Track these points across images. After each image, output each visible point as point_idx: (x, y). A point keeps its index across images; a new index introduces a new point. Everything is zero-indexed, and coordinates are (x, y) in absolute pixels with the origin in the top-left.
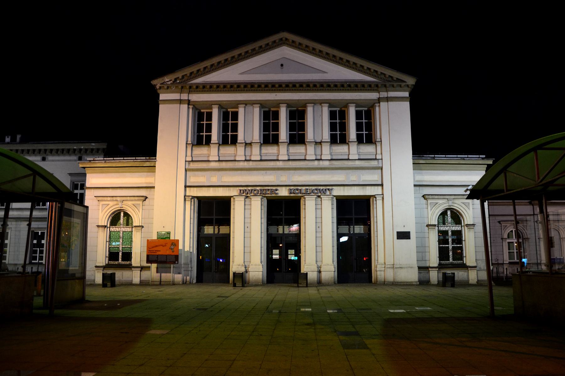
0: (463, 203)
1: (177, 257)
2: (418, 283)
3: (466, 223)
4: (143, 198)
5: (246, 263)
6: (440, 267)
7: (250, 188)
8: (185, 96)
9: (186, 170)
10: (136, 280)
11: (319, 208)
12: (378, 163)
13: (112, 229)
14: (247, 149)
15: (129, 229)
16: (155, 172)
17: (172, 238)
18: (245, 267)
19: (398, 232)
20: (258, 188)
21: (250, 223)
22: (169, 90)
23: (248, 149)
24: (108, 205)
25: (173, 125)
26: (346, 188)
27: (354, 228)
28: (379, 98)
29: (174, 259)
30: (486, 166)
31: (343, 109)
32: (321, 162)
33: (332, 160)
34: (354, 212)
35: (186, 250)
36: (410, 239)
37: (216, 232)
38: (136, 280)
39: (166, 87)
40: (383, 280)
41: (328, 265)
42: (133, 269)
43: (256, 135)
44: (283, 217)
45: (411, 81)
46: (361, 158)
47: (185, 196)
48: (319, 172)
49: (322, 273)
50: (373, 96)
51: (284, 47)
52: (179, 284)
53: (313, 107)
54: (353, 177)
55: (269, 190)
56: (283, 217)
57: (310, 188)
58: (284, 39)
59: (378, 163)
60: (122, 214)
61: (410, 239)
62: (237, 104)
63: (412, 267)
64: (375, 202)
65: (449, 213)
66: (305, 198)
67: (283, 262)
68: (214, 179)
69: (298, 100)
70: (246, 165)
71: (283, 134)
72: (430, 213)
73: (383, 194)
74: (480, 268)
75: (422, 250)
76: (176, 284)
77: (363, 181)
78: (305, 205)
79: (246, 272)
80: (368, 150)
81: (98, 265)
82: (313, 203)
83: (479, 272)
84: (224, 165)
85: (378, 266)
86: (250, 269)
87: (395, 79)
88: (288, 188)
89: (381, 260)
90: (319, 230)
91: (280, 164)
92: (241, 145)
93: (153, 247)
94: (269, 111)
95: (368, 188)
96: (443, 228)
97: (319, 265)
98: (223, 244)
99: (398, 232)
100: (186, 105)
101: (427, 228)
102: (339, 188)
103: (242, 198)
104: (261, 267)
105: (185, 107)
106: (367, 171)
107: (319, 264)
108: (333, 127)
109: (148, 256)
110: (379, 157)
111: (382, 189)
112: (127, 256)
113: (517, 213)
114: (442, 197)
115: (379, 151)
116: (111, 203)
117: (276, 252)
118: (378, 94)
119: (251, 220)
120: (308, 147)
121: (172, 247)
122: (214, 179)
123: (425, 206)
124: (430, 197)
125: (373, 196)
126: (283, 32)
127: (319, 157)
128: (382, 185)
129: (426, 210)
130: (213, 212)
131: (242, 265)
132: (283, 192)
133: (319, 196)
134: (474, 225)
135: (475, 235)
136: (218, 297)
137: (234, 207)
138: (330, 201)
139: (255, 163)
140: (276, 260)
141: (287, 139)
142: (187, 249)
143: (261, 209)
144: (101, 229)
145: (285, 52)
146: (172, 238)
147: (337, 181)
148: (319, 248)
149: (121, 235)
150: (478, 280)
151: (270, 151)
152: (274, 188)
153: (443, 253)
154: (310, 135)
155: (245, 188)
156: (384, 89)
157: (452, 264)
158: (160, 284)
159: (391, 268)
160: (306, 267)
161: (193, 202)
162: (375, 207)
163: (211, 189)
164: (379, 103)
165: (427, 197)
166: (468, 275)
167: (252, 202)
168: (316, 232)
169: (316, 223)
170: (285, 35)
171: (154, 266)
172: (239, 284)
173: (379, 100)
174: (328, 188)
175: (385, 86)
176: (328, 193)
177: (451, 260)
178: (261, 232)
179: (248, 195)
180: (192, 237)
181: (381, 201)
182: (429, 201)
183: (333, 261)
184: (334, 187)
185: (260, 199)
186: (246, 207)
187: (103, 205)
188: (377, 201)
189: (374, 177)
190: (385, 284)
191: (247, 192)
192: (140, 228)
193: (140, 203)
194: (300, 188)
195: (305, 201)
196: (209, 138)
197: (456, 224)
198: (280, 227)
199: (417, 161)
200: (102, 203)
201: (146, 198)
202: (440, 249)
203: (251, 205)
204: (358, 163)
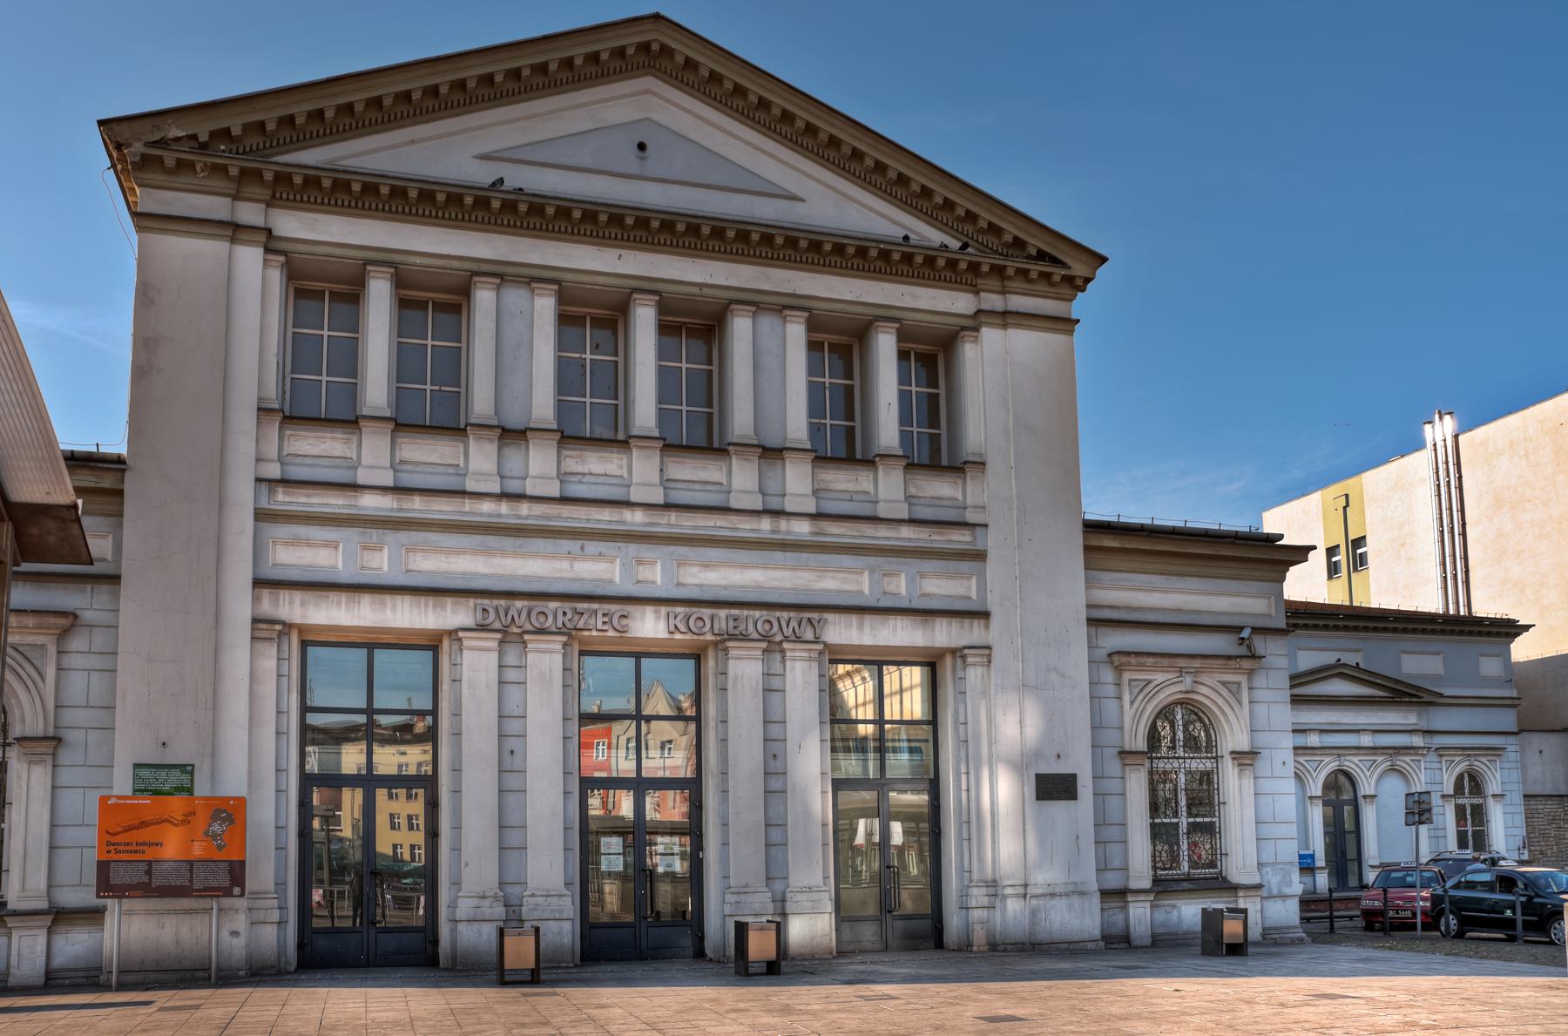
0: (1224, 683)
8: (250, 213)
26: (868, 618)
28: (979, 312)
29: (224, 881)
32: (783, 524)
33: (818, 516)
50: (957, 303)
84: (417, 506)
87: (1033, 252)
103: (491, 640)
104: (567, 901)
109: (103, 867)
113: (381, 656)
121: (216, 828)
124: (1133, 660)
131: (496, 897)
139: (539, 509)
156: (994, 283)
157: (1188, 878)
163: (366, 599)
173: (979, 318)
175: (998, 271)
177: (1185, 866)
184: (830, 617)
191: (510, 613)
199: (1094, 542)
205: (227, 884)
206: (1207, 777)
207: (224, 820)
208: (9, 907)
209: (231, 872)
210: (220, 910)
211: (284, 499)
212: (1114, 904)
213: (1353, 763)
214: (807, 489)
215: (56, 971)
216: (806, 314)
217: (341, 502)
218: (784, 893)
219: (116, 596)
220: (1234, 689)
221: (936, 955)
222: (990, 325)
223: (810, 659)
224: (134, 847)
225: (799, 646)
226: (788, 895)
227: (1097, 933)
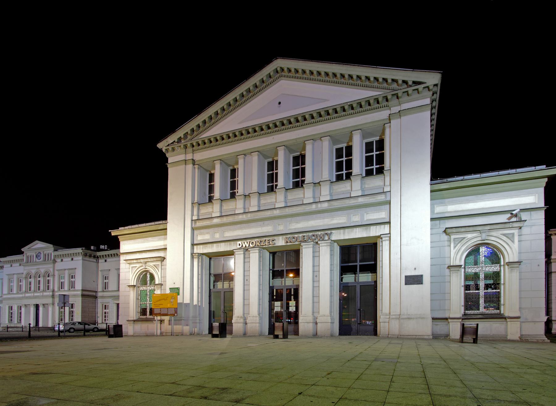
0: (504, 235)
2: (431, 337)
3: (507, 261)
11: (316, 256)
12: (386, 197)
19: (406, 277)
22: (175, 152)
26: (347, 230)
30: (546, 180)
32: (319, 205)
34: (359, 258)
36: (422, 283)
39: (170, 149)
41: (325, 316)
45: (433, 78)
48: (322, 218)
50: (383, 114)
51: (282, 81)
52: (186, 335)
53: (313, 145)
59: (386, 197)
61: (422, 283)
62: (237, 155)
70: (244, 217)
71: (381, 198)
72: (453, 251)
75: (439, 295)
76: (321, 337)
77: (367, 220)
80: (375, 182)
82: (311, 250)
83: (523, 324)
84: (225, 220)
90: (316, 279)
91: (277, 213)
92: (240, 197)
95: (372, 228)
99: (406, 277)
101: (447, 270)
102: (338, 231)
105: (190, 166)
114: (471, 229)
115: (387, 183)
116: (138, 265)
117: (277, 304)
121: (172, 300)
123: (446, 243)
124: (454, 230)
129: (447, 248)
131: (241, 317)
132: (280, 242)
134: (519, 262)
135: (520, 276)
145: (284, 87)
147: (337, 224)
148: (315, 296)
152: (271, 238)
153: (471, 302)
159: (396, 318)
163: (215, 245)
166: (506, 329)
170: (280, 63)
176: (326, 238)
181: (388, 242)
182: (453, 237)
185: (258, 251)
187: (132, 267)
189: (381, 215)
193: (159, 263)
194: (296, 236)
197: (493, 264)
200: (131, 266)
201: (164, 258)
202: (467, 298)
206: (497, 275)
210: (175, 320)
211: (199, 224)
219: (166, 252)
220: (511, 237)
223: (327, 246)
225: (323, 242)
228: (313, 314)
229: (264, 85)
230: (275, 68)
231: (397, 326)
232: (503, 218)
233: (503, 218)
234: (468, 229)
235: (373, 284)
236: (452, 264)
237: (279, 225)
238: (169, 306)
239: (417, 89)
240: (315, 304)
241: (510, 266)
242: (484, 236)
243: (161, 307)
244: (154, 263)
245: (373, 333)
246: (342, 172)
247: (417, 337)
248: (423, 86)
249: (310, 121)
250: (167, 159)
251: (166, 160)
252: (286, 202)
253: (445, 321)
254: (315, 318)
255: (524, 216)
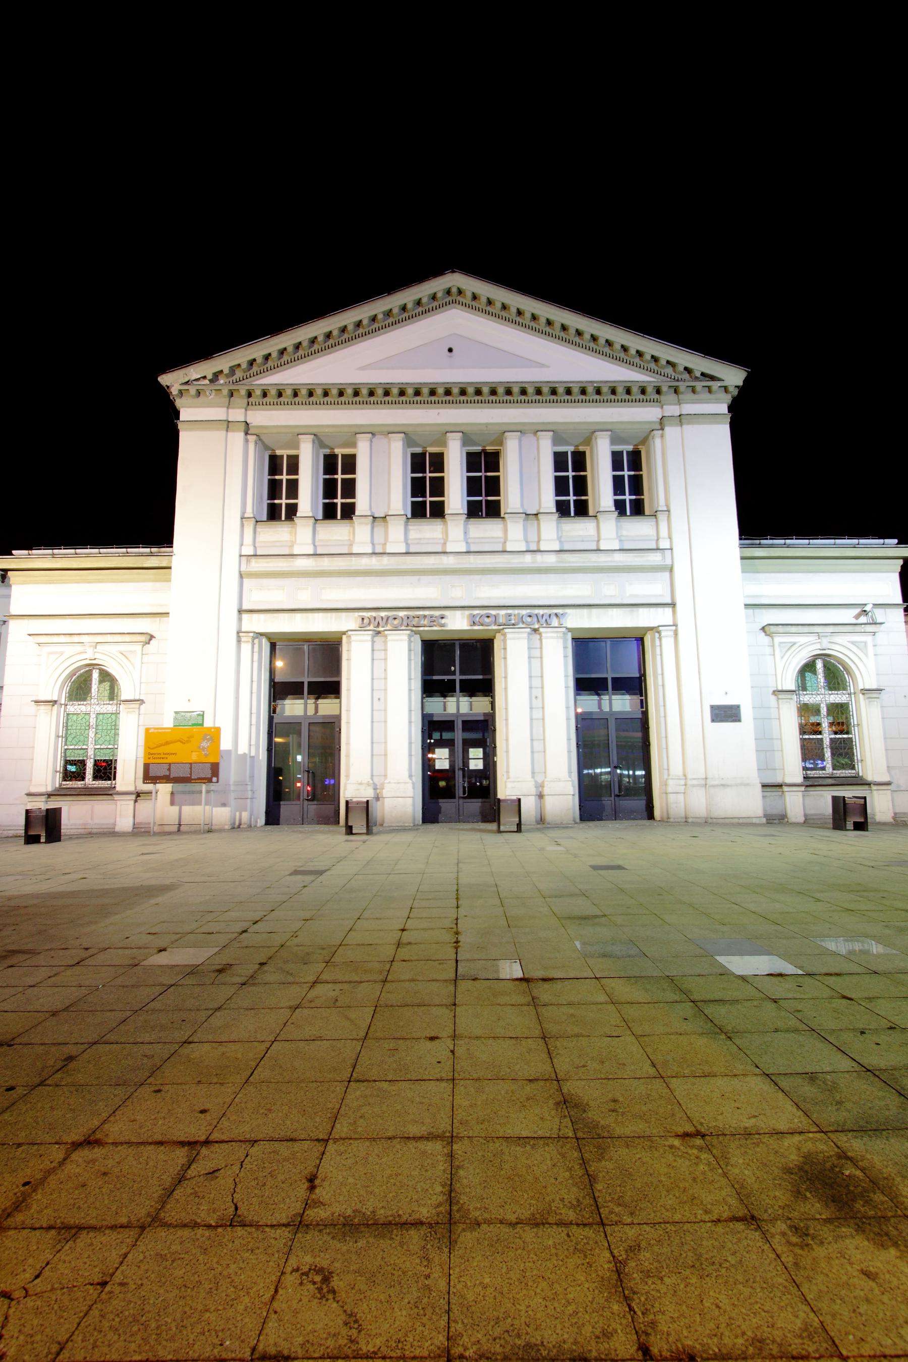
0: (853, 643)
1: (215, 769)
2: (764, 820)
3: (861, 687)
4: (147, 638)
5: (376, 780)
6: (810, 783)
7: (383, 614)
8: (237, 415)
9: (241, 576)
10: (125, 823)
11: (535, 656)
12: (664, 557)
13: (71, 709)
14: (376, 529)
15: (111, 708)
16: (169, 580)
17: (208, 723)
18: (375, 789)
20: (402, 614)
21: (386, 690)
22: (202, 399)
23: (379, 530)
24: (62, 653)
25: (212, 474)
26: (594, 611)
27: (610, 700)
30: (901, 562)
31: (581, 448)
32: (539, 557)
34: (609, 668)
35: (240, 752)
36: (739, 721)
37: (311, 711)
38: (125, 823)
39: (193, 391)
40: (683, 815)
41: (559, 780)
42: (116, 797)
43: (398, 497)
44: (458, 677)
45: (734, 376)
46: (625, 547)
47: (238, 633)
48: (533, 581)
49: (546, 797)
50: (647, 414)
52: (221, 831)
54: (610, 589)
55: (425, 616)
56: (458, 677)
57: (516, 611)
58: (454, 290)
60: (96, 675)
61: (739, 721)
62: (354, 433)
63: (747, 785)
64: (657, 643)
65: (819, 665)
66: (505, 635)
67: (459, 775)
68: (305, 595)
69: (487, 425)
72: (780, 665)
73: (675, 625)
74: (898, 786)
75: (766, 746)
78: (505, 649)
79: (377, 798)
80: (637, 529)
81: (33, 790)
84: (326, 564)
85: (670, 782)
86: (385, 793)
87: (698, 374)
88: (467, 612)
89: (676, 768)
91: (448, 561)
92: (363, 520)
93: (161, 745)
94: (423, 455)
95: (642, 611)
96: (807, 699)
97: (540, 781)
98: (326, 740)
99: (713, 707)
100: (241, 435)
101: (773, 698)
104: (410, 786)
105: (238, 437)
106: (640, 574)
107: (539, 779)
108: (561, 486)
109: (147, 767)
110: (664, 544)
111: (674, 612)
112: (105, 770)
114: (806, 629)
115: (664, 532)
116: (70, 650)
118: (658, 410)
119: (386, 684)
120: (510, 525)
121: (204, 744)
122: (304, 594)
123: (768, 650)
124: (780, 629)
125: (651, 629)
126: (453, 272)
127: (533, 547)
128: (673, 605)
130: (309, 672)
131: (368, 784)
132: (458, 624)
133: (535, 630)
136: (296, 872)
137: (349, 655)
138: (561, 641)
139: (393, 559)
140: (443, 788)
141: (462, 508)
142: (243, 749)
143: (410, 660)
144: (43, 708)
146: (208, 723)
148: (538, 742)
149: (93, 721)
150: (895, 814)
151: (428, 531)
152: (437, 613)
154: (512, 496)
155: (374, 614)
158: (179, 830)
160: (509, 785)
161: (256, 646)
162: (658, 652)
163: (298, 616)
164: (662, 429)
165: (773, 629)
167: (389, 644)
168: (531, 708)
169: (531, 688)
171: (164, 789)
172: (359, 825)
173: (662, 423)
174: (555, 611)
176: (555, 622)
178: (410, 711)
179: (381, 629)
180: (254, 722)
182: (777, 639)
183: (570, 772)
184: (568, 611)
186: (378, 655)
187: (49, 653)
188: (664, 640)
190: (686, 822)
192: (135, 705)
193: (138, 648)
194: (493, 612)
195: (505, 641)
196: (292, 511)
197: (830, 689)
198: (449, 699)
201: (152, 637)
203: (386, 650)
204: (620, 559)
205: (209, 776)
207: (208, 740)
208: (117, 789)
209: (212, 769)
210: (208, 792)
211: (257, 565)
212: (773, 794)
213: (293, 1262)
214: (554, 536)
215: (139, 824)
216: (551, 433)
217: (285, 565)
218: (543, 782)
220: (862, 646)
221: (648, 822)
222: (671, 425)
223: (557, 638)
224: (162, 756)
226: (546, 783)
227: (760, 812)
228: (533, 777)
229: (420, 310)
230: (448, 286)
231: (703, 800)
232: (848, 616)
233: (848, 616)
234: (801, 629)
235: (640, 716)
236: (780, 688)
237: (453, 586)
238: (194, 757)
239: (709, 387)
240: (536, 755)
241: (867, 696)
242: (825, 643)
243: (171, 759)
244: (123, 648)
245: (645, 814)
246: (344, 501)
247: (741, 821)
248: (719, 384)
249: (516, 396)
250: (179, 412)
251: (177, 414)
252: (407, 544)
253: (777, 789)
254: (540, 786)
255: (879, 615)
